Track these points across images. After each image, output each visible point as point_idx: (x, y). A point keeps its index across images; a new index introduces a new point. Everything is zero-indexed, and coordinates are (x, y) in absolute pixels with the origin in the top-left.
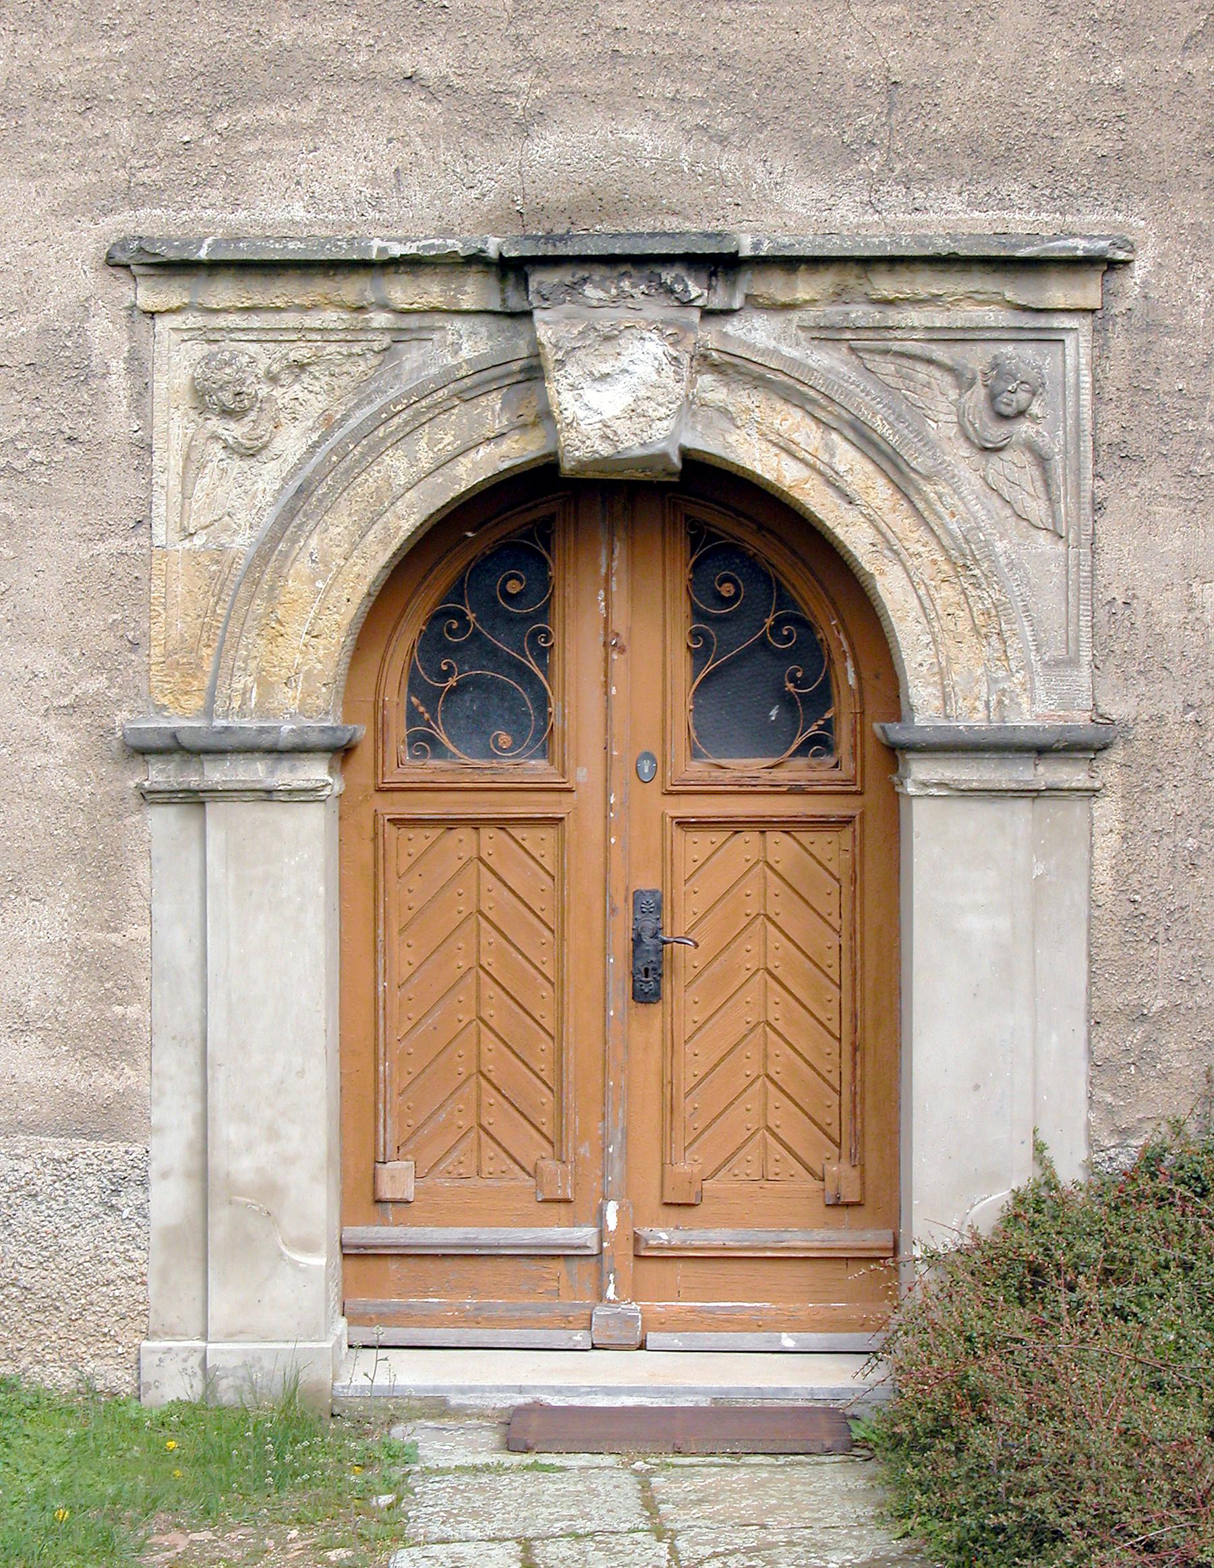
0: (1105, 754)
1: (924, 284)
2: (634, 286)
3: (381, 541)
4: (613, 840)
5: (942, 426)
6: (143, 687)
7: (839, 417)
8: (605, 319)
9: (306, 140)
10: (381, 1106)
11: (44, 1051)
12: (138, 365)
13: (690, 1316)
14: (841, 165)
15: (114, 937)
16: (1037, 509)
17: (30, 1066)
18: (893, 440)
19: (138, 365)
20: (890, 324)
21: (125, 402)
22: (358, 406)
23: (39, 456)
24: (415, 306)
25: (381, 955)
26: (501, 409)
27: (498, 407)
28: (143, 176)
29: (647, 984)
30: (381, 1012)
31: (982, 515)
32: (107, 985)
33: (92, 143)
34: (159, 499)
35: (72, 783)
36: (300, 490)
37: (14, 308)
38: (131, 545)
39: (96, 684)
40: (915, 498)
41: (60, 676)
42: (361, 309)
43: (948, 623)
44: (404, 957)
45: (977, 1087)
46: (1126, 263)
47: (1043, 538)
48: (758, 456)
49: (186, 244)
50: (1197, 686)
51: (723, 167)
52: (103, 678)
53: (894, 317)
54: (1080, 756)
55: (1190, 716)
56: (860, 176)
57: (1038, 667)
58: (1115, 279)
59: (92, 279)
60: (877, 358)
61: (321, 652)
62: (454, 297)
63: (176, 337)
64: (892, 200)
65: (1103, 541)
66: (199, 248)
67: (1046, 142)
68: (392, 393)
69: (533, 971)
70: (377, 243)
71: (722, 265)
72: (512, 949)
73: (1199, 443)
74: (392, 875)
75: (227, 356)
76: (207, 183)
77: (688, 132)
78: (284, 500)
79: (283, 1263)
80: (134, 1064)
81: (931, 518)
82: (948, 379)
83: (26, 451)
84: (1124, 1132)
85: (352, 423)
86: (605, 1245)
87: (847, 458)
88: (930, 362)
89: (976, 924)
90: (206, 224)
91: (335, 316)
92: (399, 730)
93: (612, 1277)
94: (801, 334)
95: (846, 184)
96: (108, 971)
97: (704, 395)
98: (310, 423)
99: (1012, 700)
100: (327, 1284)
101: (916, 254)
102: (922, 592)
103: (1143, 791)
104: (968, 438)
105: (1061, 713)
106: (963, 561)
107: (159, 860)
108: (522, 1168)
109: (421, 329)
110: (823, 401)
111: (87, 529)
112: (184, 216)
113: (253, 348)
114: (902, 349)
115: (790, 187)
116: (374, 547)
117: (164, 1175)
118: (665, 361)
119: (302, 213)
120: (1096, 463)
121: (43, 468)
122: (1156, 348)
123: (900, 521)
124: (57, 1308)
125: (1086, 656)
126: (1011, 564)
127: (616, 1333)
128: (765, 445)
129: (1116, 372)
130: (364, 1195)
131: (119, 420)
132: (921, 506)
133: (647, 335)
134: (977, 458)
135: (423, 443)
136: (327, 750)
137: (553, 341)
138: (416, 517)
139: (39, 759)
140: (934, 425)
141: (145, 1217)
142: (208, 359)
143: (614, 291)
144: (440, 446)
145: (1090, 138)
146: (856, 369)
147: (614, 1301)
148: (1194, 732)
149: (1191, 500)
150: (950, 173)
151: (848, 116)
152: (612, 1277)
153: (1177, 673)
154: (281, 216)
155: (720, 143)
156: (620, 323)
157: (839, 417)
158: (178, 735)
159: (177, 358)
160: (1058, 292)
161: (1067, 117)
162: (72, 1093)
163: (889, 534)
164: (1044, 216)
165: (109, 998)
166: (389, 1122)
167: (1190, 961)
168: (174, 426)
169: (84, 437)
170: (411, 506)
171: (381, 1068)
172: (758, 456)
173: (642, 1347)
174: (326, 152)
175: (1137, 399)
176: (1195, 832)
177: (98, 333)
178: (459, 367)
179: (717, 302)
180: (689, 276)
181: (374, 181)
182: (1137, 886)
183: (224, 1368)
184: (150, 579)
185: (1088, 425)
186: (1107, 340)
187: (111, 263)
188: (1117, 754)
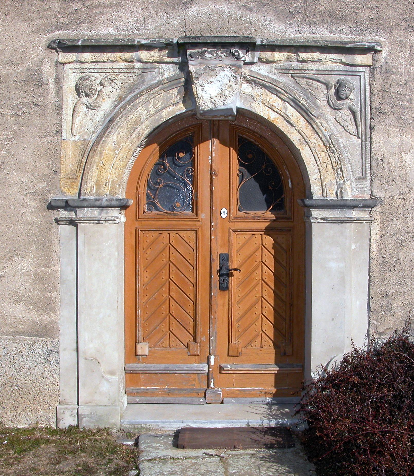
0: (374, 209)
1: (316, 55)
2: (222, 53)
3: (137, 137)
4: (213, 237)
5: (322, 102)
6: (58, 186)
7: (288, 98)
8: (213, 63)
9: (115, 9)
10: (138, 324)
11: (25, 308)
12: (58, 80)
13: (238, 392)
14: (289, 19)
15: (48, 270)
16: (352, 128)
17: (20, 313)
18: (306, 105)
19: (58, 80)
20: (305, 68)
21: (54, 92)
22: (130, 93)
23: (25, 110)
24: (149, 61)
25: (137, 275)
26: (177, 95)
27: (176, 94)
28: (62, 20)
29: (224, 287)
30: (138, 294)
31: (335, 130)
32: (46, 286)
33: (45, 10)
34: (64, 124)
35: (34, 218)
36: (110, 121)
37: (18, 62)
38: (55, 139)
39: (42, 185)
40: (313, 124)
41: (31, 182)
42: (132, 62)
43: (324, 166)
44: (145, 276)
45: (333, 319)
46: (380, 51)
47: (354, 139)
48: (262, 110)
49: (74, 41)
50: (404, 187)
51: (251, 18)
52: (45, 183)
53: (306, 66)
54: (367, 209)
55: (401, 197)
56: (295, 22)
57: (353, 180)
58: (378, 56)
59: (42, 52)
60: (301, 79)
61: (117, 174)
62: (162, 57)
63: (70, 71)
64: (305, 30)
65: (374, 139)
66: (79, 41)
67: (354, 14)
68: (141, 89)
69: (187, 280)
70: (137, 40)
71: (249, 46)
72: (180, 273)
73: (404, 109)
74: (141, 248)
75: (87, 77)
76: (82, 22)
77: (240, 7)
78: (105, 124)
79: (103, 379)
80: (55, 312)
81: (318, 131)
82: (324, 86)
83: (21, 108)
84: (380, 334)
85: (128, 98)
86: (210, 370)
87: (291, 112)
88: (318, 81)
89: (333, 265)
90: (82, 33)
91: (123, 64)
92: (144, 200)
93: (212, 380)
94: (276, 71)
95: (291, 24)
96: (45, 280)
97: (244, 90)
98: (114, 99)
99: (345, 191)
100: (119, 385)
101: (314, 45)
102: (315, 155)
103: (387, 221)
104: (330, 106)
105: (361, 195)
106: (330, 145)
107: (62, 244)
108: (184, 344)
109: (151, 68)
110: (284, 93)
111: (41, 134)
112: (75, 32)
113: (96, 75)
114: (309, 77)
115: (272, 25)
116: (135, 140)
117: (65, 350)
118: (231, 78)
119: (113, 31)
120: (371, 114)
121: (27, 114)
122: (390, 78)
123: (308, 132)
124: (30, 394)
125: (369, 177)
126: (344, 147)
127: (213, 399)
128: (264, 107)
129: (377, 86)
130: (132, 353)
131: (52, 97)
132: (315, 127)
133: (226, 69)
134: (333, 111)
135: (151, 105)
136: (118, 207)
137: (195, 71)
138: (149, 129)
139: (23, 210)
140: (319, 101)
141: (58, 363)
142: (81, 79)
143: (215, 55)
144: (157, 106)
145: (368, 13)
146: (294, 83)
147: (213, 388)
148: (403, 202)
149: (401, 127)
150: (324, 22)
151: (291, 3)
152: (212, 380)
153: (398, 183)
154: (106, 32)
155: (250, 11)
156: (217, 65)
157: (288, 98)
158: (69, 202)
159: (71, 78)
160: (359, 59)
161: (360, 6)
162: (34, 322)
163: (305, 136)
164: (354, 37)
165: (45, 290)
166: (140, 330)
167: (401, 277)
168: (70, 98)
169: (40, 104)
170: (147, 126)
171: (138, 312)
172: (262, 110)
173: (222, 402)
174: (121, 12)
175: (384, 94)
176: (403, 235)
177: (45, 70)
178: (163, 80)
179: (248, 60)
180: (240, 49)
181: (137, 22)
182: (385, 252)
183: (84, 415)
184: (61, 150)
185: (368, 102)
186: (374, 75)
187: (50, 47)
188: (378, 209)
